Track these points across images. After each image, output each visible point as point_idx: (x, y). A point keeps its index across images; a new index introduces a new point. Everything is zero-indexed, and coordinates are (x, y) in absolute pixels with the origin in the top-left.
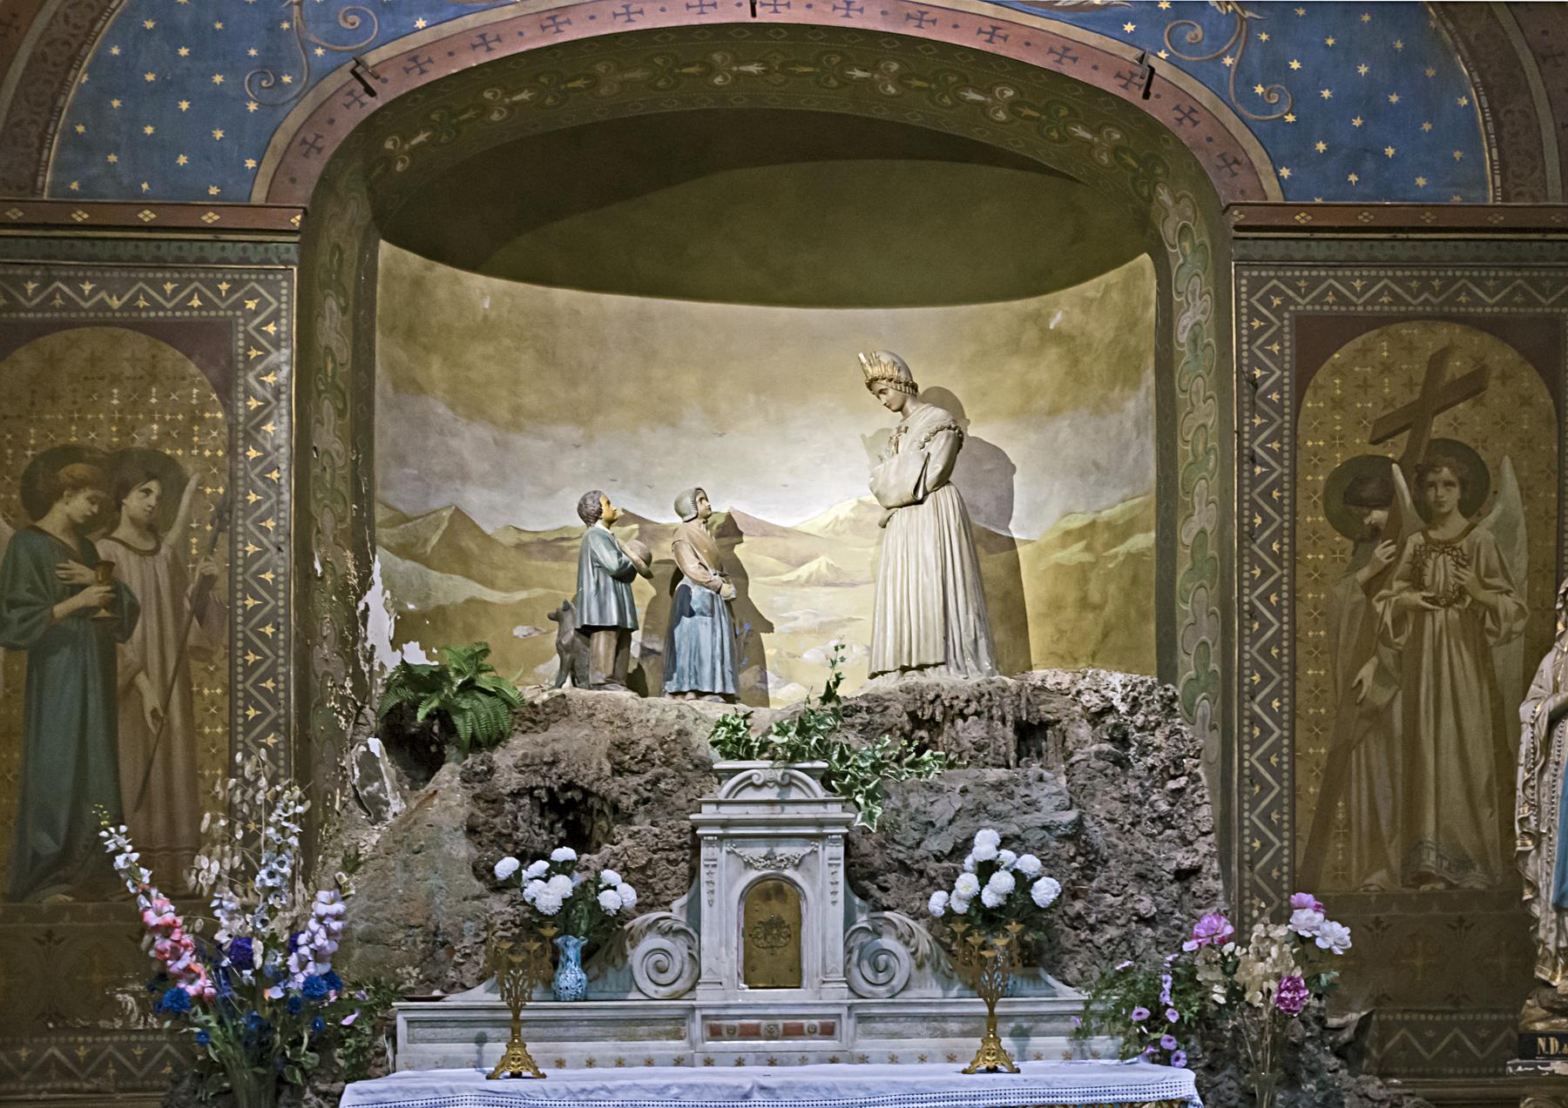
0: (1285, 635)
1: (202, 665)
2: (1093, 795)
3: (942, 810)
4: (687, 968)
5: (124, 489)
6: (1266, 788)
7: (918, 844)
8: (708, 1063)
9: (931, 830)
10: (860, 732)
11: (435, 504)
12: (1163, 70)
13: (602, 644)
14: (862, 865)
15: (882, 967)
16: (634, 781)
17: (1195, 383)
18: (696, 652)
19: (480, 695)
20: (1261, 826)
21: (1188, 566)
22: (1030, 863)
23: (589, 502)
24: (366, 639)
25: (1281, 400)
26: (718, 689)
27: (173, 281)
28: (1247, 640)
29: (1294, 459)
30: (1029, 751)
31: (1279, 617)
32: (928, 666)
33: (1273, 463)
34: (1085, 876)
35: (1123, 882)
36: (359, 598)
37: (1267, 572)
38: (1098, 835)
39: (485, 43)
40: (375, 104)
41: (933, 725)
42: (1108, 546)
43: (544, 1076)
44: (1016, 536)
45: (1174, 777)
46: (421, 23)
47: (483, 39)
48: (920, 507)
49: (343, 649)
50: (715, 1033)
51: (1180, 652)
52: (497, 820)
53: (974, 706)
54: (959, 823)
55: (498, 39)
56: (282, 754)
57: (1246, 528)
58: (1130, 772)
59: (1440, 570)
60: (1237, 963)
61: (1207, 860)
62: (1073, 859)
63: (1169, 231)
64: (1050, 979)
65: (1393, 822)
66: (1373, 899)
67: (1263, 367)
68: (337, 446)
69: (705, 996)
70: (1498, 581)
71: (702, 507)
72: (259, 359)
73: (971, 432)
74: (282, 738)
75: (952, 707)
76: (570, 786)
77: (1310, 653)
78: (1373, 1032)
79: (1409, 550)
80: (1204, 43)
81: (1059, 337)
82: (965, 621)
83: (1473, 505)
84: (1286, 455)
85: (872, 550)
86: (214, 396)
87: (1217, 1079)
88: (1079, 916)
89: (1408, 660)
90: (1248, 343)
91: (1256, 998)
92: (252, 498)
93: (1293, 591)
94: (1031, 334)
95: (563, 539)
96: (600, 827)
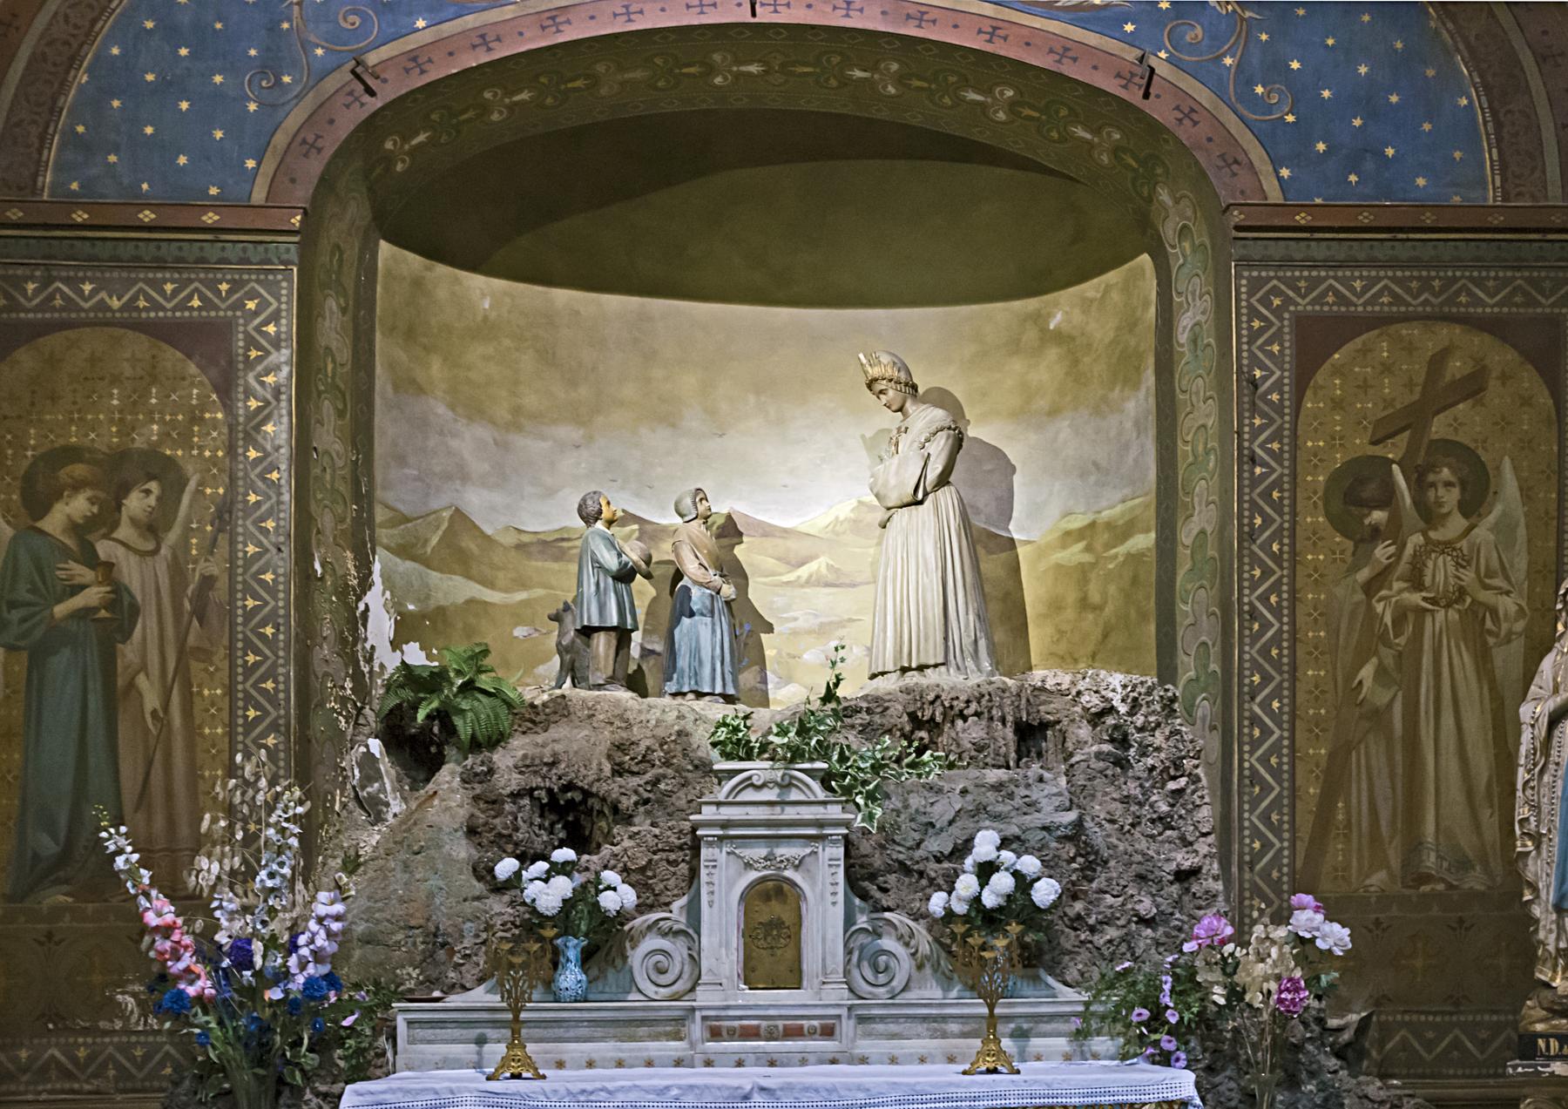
0: (1285, 636)
1: (202, 666)
2: (1093, 796)
3: (942, 811)
4: (687, 968)
5: (124, 490)
6: (1266, 789)
7: (918, 845)
8: (708, 1064)
9: (931, 831)
10: (860, 732)
11: (435, 504)
12: (1163, 70)
13: (602, 645)
14: (862, 866)
15: (882, 968)
16: (634, 781)
17: (1195, 384)
18: (696, 653)
19: (480, 696)
20: (1261, 827)
21: (1188, 566)
22: (1030, 864)
23: (589, 502)
24: (366, 639)
25: (1281, 400)
26: (718, 690)
27: (173, 281)
28: (1247, 640)
29: (1294, 459)
30: (1029, 752)
31: (1279, 617)
32: (928, 667)
33: (1273, 464)
34: (1085, 877)
35: (1123, 882)
36: (359, 599)
37: (1267, 573)
38: (1098, 836)
39: (485, 43)
40: (375, 104)
41: (933, 726)
42: (1108, 546)
43: (544, 1077)
44: (1016, 536)
45: (1174, 778)
46: (421, 24)
47: (483, 39)
48: (920, 507)
49: (343, 649)
50: (715, 1034)
51: (1180, 652)
52: (497, 821)
53: (974, 706)
54: (959, 824)
55: (498, 39)
56: (282, 755)
57: (1246, 529)
58: (1130, 773)
59: (1440, 571)
60: (1237, 964)
61: (1207, 861)
62: (1073, 860)
63: (1169, 231)
64: (1050, 980)
65: (1393, 823)
66: (1373, 900)
67: (1263, 367)
68: (337, 447)
69: (705, 997)
70: (1498, 582)
71: (702, 508)
72: (259, 359)
73: (971, 432)
74: (282, 739)
75: (952, 707)
76: (570, 786)
77: (1310, 653)
78: (1373, 1033)
79: (1409, 550)
80: (1204, 43)
81: (1059, 337)
82: (965, 622)
83: (1473, 506)
84: (1286, 456)
85: (872, 551)
86: (214, 396)
87: (1217, 1080)
88: (1079, 917)
89: (1408, 661)
90: (1248, 343)
91: (1256, 999)
92: (252, 498)
93: (1293, 591)
94: (1031, 335)
95: (563, 540)
96: (600, 828)
